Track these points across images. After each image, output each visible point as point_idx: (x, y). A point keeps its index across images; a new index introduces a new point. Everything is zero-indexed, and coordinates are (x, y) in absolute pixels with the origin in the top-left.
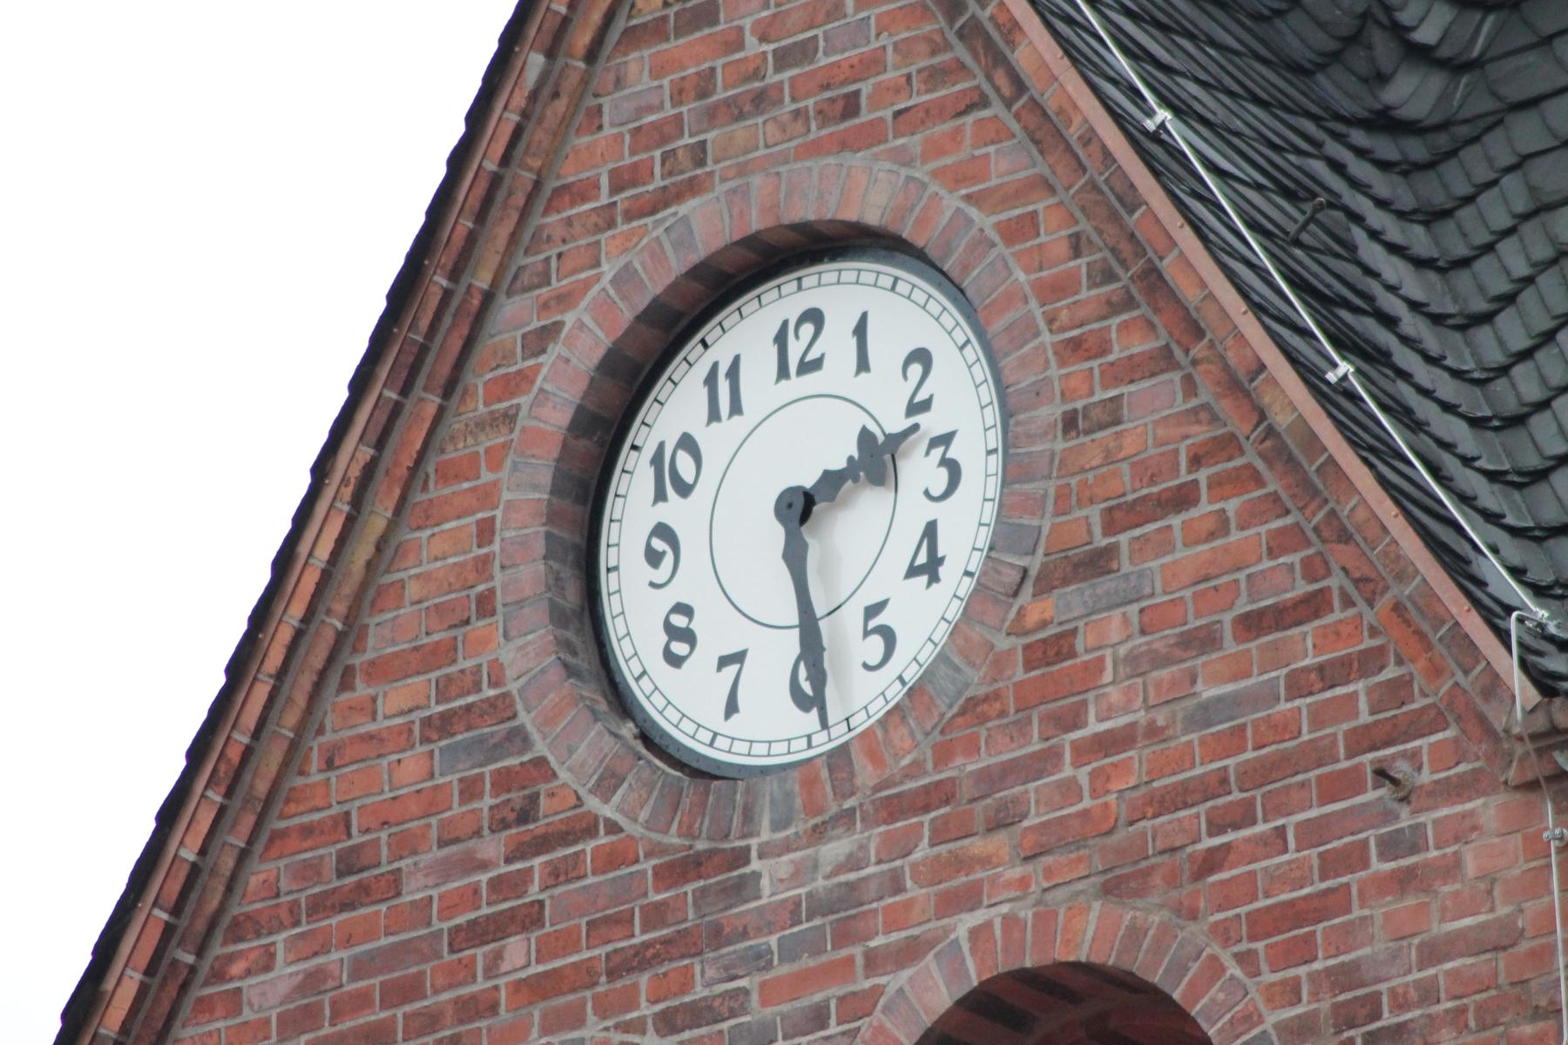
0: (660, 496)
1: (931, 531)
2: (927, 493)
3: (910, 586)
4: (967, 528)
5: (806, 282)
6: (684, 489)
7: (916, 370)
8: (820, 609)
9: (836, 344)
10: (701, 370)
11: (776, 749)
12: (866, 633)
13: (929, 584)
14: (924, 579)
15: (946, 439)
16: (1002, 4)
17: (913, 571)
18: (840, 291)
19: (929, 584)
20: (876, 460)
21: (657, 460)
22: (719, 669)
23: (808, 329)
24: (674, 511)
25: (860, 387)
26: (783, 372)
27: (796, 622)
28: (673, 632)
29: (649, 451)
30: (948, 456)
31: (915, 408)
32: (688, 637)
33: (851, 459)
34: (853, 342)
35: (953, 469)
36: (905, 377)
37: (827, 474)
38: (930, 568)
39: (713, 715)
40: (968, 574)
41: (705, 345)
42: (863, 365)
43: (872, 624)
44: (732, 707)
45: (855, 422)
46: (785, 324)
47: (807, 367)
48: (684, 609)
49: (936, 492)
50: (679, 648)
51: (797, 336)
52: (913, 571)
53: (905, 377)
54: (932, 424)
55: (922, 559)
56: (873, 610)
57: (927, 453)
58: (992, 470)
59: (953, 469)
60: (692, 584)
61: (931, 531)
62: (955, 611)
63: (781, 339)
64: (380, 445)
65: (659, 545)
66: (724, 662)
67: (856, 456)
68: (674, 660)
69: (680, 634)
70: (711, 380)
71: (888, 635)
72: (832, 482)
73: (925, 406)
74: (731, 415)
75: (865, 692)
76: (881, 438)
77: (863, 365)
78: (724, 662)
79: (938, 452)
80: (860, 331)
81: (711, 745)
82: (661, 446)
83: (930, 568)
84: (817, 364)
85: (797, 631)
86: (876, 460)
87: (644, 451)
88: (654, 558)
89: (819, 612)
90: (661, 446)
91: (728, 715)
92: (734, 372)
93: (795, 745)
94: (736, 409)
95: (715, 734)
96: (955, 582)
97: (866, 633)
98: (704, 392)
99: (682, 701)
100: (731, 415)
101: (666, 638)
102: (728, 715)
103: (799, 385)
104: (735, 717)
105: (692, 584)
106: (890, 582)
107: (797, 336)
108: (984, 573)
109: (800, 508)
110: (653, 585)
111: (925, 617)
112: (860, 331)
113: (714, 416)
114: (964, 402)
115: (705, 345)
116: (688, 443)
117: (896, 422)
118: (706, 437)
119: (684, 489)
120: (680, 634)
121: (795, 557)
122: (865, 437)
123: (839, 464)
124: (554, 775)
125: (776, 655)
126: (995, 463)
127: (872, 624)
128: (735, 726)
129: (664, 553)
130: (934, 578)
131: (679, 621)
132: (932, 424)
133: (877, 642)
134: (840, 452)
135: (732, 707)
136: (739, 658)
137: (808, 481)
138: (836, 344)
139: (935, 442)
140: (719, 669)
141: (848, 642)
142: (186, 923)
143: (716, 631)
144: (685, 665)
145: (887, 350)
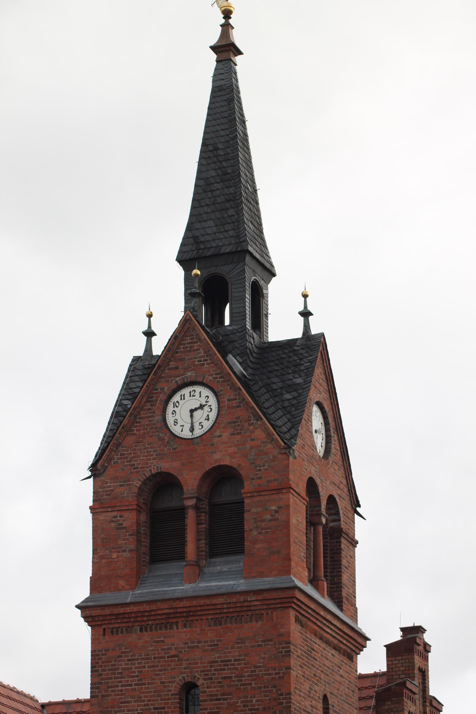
0: (174, 407)
1: (208, 415)
3: (205, 421)
4: (213, 416)
7: (207, 398)
9: (197, 394)
10: (180, 394)
15: (210, 406)
17: (206, 419)
20: (201, 407)
23: (194, 392)
24: (175, 409)
25: (200, 399)
26: (190, 396)
28: (175, 422)
29: (173, 402)
31: (206, 402)
32: (177, 423)
38: (208, 419)
39: (180, 432)
42: (200, 396)
44: (182, 431)
47: (193, 396)
48: (177, 420)
50: (176, 424)
54: (209, 404)
56: (200, 423)
60: (177, 417)
61: (208, 415)
63: (190, 392)
64: (141, 399)
66: (181, 426)
68: (175, 425)
69: (176, 422)
70: (181, 396)
72: (196, 409)
73: (208, 402)
75: (198, 432)
77: (200, 396)
78: (181, 426)
80: (200, 393)
84: (195, 396)
88: (173, 414)
92: (184, 395)
94: (184, 399)
99: (176, 430)
103: (192, 398)
105: (177, 417)
106: (203, 420)
108: (312, 437)
109: (192, 411)
111: (207, 425)
112: (200, 393)
113: (181, 399)
114: (213, 401)
117: (204, 403)
118: (180, 401)
119: (177, 407)
120: (176, 422)
121: (192, 416)
122: (201, 405)
125: (187, 427)
130: (208, 421)
131: (176, 421)
132: (209, 404)
133: (201, 427)
134: (198, 406)
135: (182, 431)
136: (183, 426)
137: (193, 408)
138: (197, 394)
141: (197, 426)
142: (181, 631)
143: (180, 423)
145: (203, 395)
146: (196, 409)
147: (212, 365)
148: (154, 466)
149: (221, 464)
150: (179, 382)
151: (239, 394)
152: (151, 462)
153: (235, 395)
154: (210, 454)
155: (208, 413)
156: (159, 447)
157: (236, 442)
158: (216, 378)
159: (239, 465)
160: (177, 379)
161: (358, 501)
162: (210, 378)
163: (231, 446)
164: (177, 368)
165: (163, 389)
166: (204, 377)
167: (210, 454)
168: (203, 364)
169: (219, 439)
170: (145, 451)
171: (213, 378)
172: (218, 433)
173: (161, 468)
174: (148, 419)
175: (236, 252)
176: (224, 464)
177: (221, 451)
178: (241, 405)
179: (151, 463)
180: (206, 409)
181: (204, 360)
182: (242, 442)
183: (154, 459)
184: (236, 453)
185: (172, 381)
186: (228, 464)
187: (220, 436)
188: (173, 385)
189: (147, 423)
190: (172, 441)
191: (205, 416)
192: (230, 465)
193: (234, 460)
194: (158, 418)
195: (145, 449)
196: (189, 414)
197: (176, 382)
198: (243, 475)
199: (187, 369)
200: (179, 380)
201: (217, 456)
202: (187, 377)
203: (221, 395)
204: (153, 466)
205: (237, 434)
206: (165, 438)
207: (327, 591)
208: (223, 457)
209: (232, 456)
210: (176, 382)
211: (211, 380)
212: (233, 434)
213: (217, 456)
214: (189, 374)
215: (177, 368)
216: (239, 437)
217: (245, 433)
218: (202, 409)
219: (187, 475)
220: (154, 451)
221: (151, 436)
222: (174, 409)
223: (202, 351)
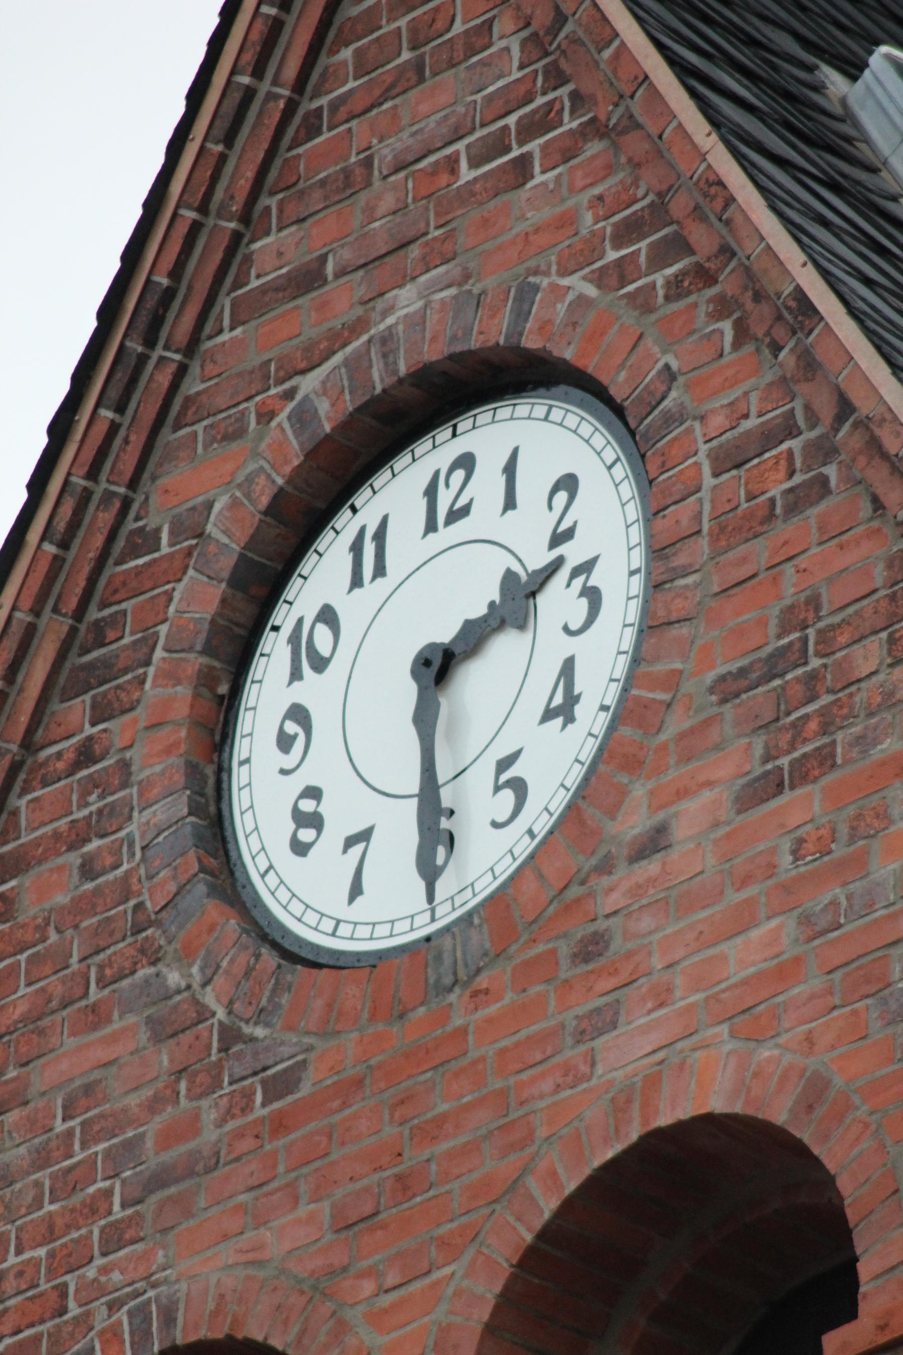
0: (296, 675)
1: (568, 668)
2: (566, 629)
3: (534, 734)
4: (604, 661)
5: (460, 428)
6: (320, 664)
8: (442, 775)
9: (487, 486)
11: (400, 927)
12: (497, 789)
13: (564, 726)
14: (560, 720)
15: (587, 568)
16: (596, 5)
17: (548, 715)
18: (493, 433)
19: (564, 726)
20: (518, 599)
21: (294, 639)
22: (345, 851)
24: (313, 691)
26: (431, 526)
27: (416, 790)
28: (302, 819)
29: (287, 630)
30: (590, 583)
32: (315, 821)
33: (492, 605)
34: (502, 481)
35: (593, 596)
36: (550, 508)
37: (468, 625)
40: (604, 708)
41: (354, 510)
42: (510, 503)
43: (503, 778)
44: (356, 890)
45: (504, 562)
46: (437, 474)
49: (574, 627)
50: (307, 835)
51: (447, 485)
52: (548, 715)
53: (550, 508)
54: (574, 553)
55: (558, 700)
56: (504, 764)
57: (568, 585)
58: (634, 591)
59: (593, 596)
61: (568, 668)
62: (589, 749)
63: (431, 492)
65: (291, 727)
66: (350, 842)
67: (498, 602)
68: (300, 849)
70: (357, 548)
71: (519, 787)
72: (474, 638)
74: (374, 577)
75: (489, 853)
76: (524, 577)
77: (510, 503)
79: (578, 582)
80: (510, 470)
81: (333, 934)
82: (300, 621)
83: (563, 710)
85: (415, 801)
86: (518, 599)
87: (282, 630)
88: (285, 742)
89: (441, 780)
90: (300, 621)
91: (352, 899)
92: (380, 536)
93: (418, 921)
94: (380, 570)
95: (338, 922)
96: (591, 720)
97: (497, 789)
98: (349, 558)
100: (374, 577)
101: (293, 826)
102: (352, 899)
103: (446, 535)
104: (359, 900)
105: (323, 764)
107: (447, 485)
109: (438, 667)
110: (284, 772)
111: (557, 763)
112: (510, 470)
113: (357, 581)
114: (610, 525)
115: (354, 510)
116: (328, 616)
121: (425, 719)
122: (509, 577)
123: (479, 610)
124: (73, 1034)
125: (399, 830)
126: (637, 584)
127: (503, 778)
128: (362, 909)
129: (295, 737)
130: (570, 719)
131: (307, 806)
132: (574, 553)
133: (508, 797)
134: (479, 596)
135: (356, 890)
136: (365, 836)
137: (445, 634)
138: (487, 486)
139: (576, 572)
140: (345, 851)
141: (476, 802)
143: (342, 814)
144: (312, 852)
145: (533, 484)
146: (474, 638)
147: (594, 147)
148: (113, 1306)
149: (663, 1120)
150: (323, 407)
151: (809, 365)
152: (91, 1272)
153: (784, 385)
154: (572, 1053)
155: (571, 646)
156: (154, 1106)
157: (787, 859)
158: (622, 272)
159: (815, 1090)
160: (308, 383)
161: (384, 568)
162: (579, 284)
163: (742, 920)
164: (308, 279)
165: (191, 527)
166: (526, 294)
167: (572, 1053)
168: (523, 167)
169: (652, 867)
170: (44, 1176)
171: (599, 279)
172: (634, 823)
173: (168, 1319)
174: (74, 859)
175: (867, 1216)
176: (685, 1111)
177: (662, 996)
178: (831, 471)
179: (95, 1289)
180: (559, 603)
181: (530, 129)
182: (839, 851)
183: (115, 1238)
184: (786, 972)
185: (266, 416)
186: (717, 1105)
187: (654, 842)
188: (272, 456)
189: (62, 899)
190: (261, 1016)
191: (542, 687)
192: (738, 1108)
193: (766, 1053)
194: (160, 814)
195: (42, 1159)
196: (409, 691)
197: (303, 418)
198: (845, 1185)
199: (386, 262)
200: (324, 389)
201: (624, 1054)
202: (387, 340)
203: (671, 420)
204: (101, 1319)
205: (802, 774)
206: (209, 998)
207: (526, 115)
208: (675, 1057)
209: (749, 1017)
210: (303, 418)
211: (582, 301)
212: (770, 786)
213: (624, 1054)
214: (407, 299)
215: (308, 279)
216: (804, 806)
217: (862, 742)
218: (522, 626)
219: (377, 1319)
220: (115, 1162)
221: (97, 1016)
222: (301, 693)
223: (508, 43)
